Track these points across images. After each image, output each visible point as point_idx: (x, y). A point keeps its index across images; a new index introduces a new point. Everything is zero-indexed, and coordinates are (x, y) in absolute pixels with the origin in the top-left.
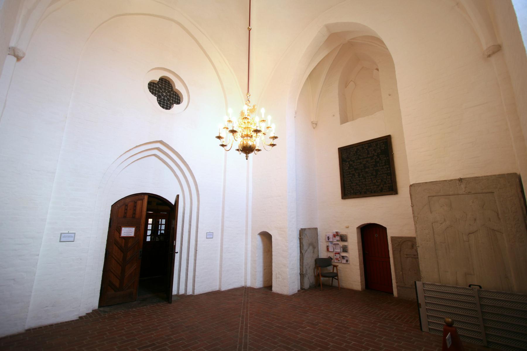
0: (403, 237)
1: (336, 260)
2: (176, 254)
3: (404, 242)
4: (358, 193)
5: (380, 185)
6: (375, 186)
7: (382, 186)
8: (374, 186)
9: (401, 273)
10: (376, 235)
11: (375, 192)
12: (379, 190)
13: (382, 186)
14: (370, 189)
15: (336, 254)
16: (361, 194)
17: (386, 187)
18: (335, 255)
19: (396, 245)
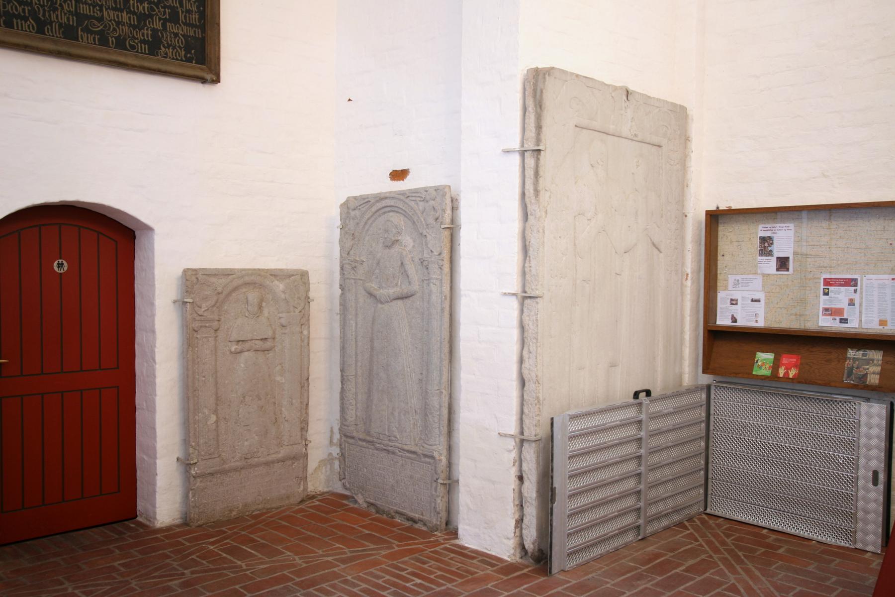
0: (231, 270)
1: (830, 318)
2: (720, 209)
3: (236, 289)
4: (26, 19)
5: (151, 16)
6: (125, 17)
7: (158, 25)
8: (121, 11)
9: (213, 418)
10: (60, 265)
11: (121, 44)
12: (142, 42)
13: (158, 25)
14: (100, 19)
15: (831, 288)
16: (41, 31)
17: (176, 35)
18: (826, 294)
19: (204, 306)
